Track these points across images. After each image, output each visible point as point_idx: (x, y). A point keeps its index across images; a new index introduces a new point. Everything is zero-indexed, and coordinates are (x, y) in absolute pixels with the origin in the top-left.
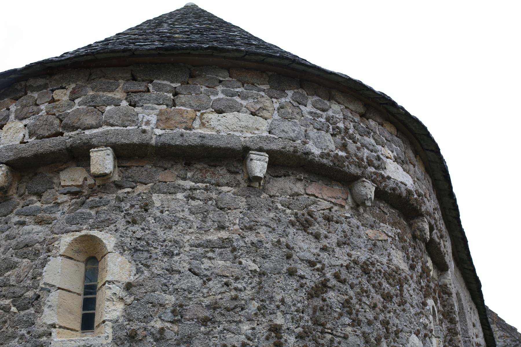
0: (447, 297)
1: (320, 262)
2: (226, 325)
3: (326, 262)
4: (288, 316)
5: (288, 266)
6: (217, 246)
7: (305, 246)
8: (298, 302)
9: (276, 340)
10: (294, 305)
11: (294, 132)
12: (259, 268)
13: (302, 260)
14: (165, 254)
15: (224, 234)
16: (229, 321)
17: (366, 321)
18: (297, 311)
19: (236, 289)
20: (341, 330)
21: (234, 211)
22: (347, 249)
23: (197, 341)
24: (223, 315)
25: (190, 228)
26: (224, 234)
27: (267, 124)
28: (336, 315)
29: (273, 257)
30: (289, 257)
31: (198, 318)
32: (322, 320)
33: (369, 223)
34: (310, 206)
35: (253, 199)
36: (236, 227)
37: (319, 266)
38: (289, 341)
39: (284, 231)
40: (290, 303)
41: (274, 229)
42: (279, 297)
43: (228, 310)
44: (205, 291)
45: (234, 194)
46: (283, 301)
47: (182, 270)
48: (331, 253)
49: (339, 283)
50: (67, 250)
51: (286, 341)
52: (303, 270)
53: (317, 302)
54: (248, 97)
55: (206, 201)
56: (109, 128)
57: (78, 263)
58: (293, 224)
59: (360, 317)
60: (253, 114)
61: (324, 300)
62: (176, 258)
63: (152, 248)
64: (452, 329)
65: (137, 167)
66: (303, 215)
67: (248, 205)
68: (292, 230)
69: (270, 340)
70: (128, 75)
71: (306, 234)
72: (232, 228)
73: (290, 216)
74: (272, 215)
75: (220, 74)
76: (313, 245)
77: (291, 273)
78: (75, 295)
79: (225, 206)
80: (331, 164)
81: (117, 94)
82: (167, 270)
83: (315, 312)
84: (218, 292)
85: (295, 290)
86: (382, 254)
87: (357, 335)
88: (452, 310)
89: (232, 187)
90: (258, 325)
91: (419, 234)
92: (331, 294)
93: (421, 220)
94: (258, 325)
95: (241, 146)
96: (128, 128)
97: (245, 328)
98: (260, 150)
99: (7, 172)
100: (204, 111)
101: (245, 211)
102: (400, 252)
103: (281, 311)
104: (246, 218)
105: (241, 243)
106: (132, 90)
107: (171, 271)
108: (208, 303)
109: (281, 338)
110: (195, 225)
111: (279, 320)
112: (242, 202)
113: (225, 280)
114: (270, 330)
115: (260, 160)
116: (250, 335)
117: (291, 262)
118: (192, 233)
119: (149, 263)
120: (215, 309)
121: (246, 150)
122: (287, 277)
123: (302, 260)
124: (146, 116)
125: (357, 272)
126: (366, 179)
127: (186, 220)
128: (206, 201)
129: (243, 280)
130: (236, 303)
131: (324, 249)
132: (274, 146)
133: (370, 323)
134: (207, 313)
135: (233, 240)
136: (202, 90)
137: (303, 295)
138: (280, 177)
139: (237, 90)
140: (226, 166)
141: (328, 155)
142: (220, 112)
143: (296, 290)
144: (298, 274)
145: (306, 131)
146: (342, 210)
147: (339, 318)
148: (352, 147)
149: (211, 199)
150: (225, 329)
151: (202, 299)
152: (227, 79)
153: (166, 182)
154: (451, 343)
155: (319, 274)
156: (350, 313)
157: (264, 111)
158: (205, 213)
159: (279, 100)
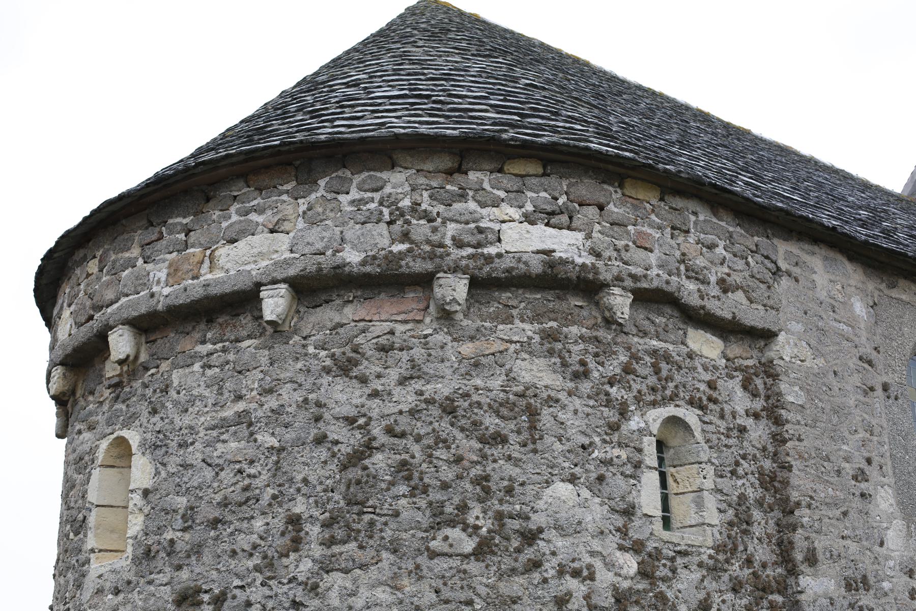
0: (772, 382)
1: (364, 415)
2: (238, 524)
3: (374, 414)
4: (311, 500)
5: (316, 431)
6: (232, 424)
7: (342, 397)
8: (327, 478)
9: (294, 534)
10: (321, 483)
11: (322, 241)
12: (279, 442)
13: (337, 419)
14: (180, 446)
15: (241, 406)
16: (240, 518)
17: (438, 483)
18: (325, 491)
19: (249, 476)
20: (391, 505)
21: (254, 372)
22: (417, 385)
23: (207, 549)
24: (234, 512)
25: (206, 406)
26: (241, 406)
27: (288, 241)
28: (384, 486)
29: (296, 424)
30: (318, 419)
31: (208, 521)
32: (360, 497)
33: (468, 333)
34: (356, 337)
35: (278, 348)
36: (254, 393)
37: (361, 421)
38: (311, 533)
39: (314, 384)
40: (315, 482)
41: (300, 385)
42: (299, 477)
43: (240, 505)
44: (215, 485)
45: (256, 348)
46: (305, 481)
47: (195, 463)
48: (385, 397)
49: (392, 439)
50: (104, 458)
51: (307, 533)
52: (337, 431)
53: (354, 473)
54: (265, 209)
55: (222, 366)
56: (127, 299)
57: (122, 470)
58: (327, 370)
59: (426, 480)
60: (272, 231)
61: (365, 468)
62: (191, 449)
63: (169, 441)
64: (777, 435)
65: (162, 338)
66: (344, 353)
67: (271, 358)
68: (326, 379)
69: (287, 535)
70: (144, 222)
71: (347, 379)
72: (248, 396)
73: (325, 359)
74: (299, 365)
75: (234, 188)
76: (358, 393)
77: (320, 440)
78: (120, 509)
79: (243, 368)
80: (379, 270)
81: (134, 251)
82: (181, 466)
83: (348, 487)
84: (231, 483)
85: (322, 462)
86: (493, 375)
87: (419, 509)
88: (778, 403)
89: (255, 338)
90: (273, 518)
91: (608, 315)
92: (378, 457)
93: (607, 292)
94: (273, 518)
95: (250, 284)
96: (142, 293)
97: (259, 524)
98: (274, 282)
99: (64, 374)
100: (215, 247)
101: (267, 368)
102: (541, 362)
103: (303, 494)
104: (268, 378)
105: (260, 413)
106: (146, 242)
107: (185, 466)
108: (219, 500)
109: (301, 530)
110: (210, 402)
111: (299, 507)
112: (264, 357)
113: (237, 466)
114: (287, 523)
115: (272, 297)
116: (262, 533)
117: (321, 424)
118: (207, 412)
119: (164, 461)
120: (226, 506)
121: (258, 285)
122: (313, 447)
123: (337, 419)
124: (157, 273)
125: (431, 415)
126: (445, 272)
127: (201, 397)
128: (222, 366)
129: (258, 462)
130: (248, 494)
131: (375, 394)
132: (292, 272)
133: (445, 486)
134: (217, 514)
135: (251, 411)
136: (214, 217)
137: (334, 467)
138: (321, 305)
139: (252, 204)
140: (251, 312)
141: (374, 258)
142: (232, 241)
143: (325, 462)
144: (330, 439)
145: (342, 232)
146: (420, 326)
147: (388, 489)
148: (420, 229)
149: (227, 363)
150: (236, 530)
151: (213, 495)
152: (243, 191)
153: (184, 352)
154: (776, 458)
155: (360, 433)
156: (409, 478)
157: (286, 223)
158: (221, 383)
159: (308, 199)
